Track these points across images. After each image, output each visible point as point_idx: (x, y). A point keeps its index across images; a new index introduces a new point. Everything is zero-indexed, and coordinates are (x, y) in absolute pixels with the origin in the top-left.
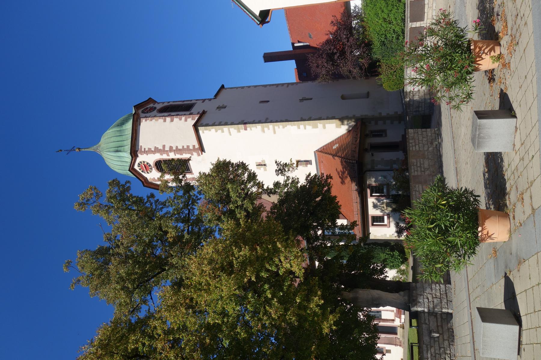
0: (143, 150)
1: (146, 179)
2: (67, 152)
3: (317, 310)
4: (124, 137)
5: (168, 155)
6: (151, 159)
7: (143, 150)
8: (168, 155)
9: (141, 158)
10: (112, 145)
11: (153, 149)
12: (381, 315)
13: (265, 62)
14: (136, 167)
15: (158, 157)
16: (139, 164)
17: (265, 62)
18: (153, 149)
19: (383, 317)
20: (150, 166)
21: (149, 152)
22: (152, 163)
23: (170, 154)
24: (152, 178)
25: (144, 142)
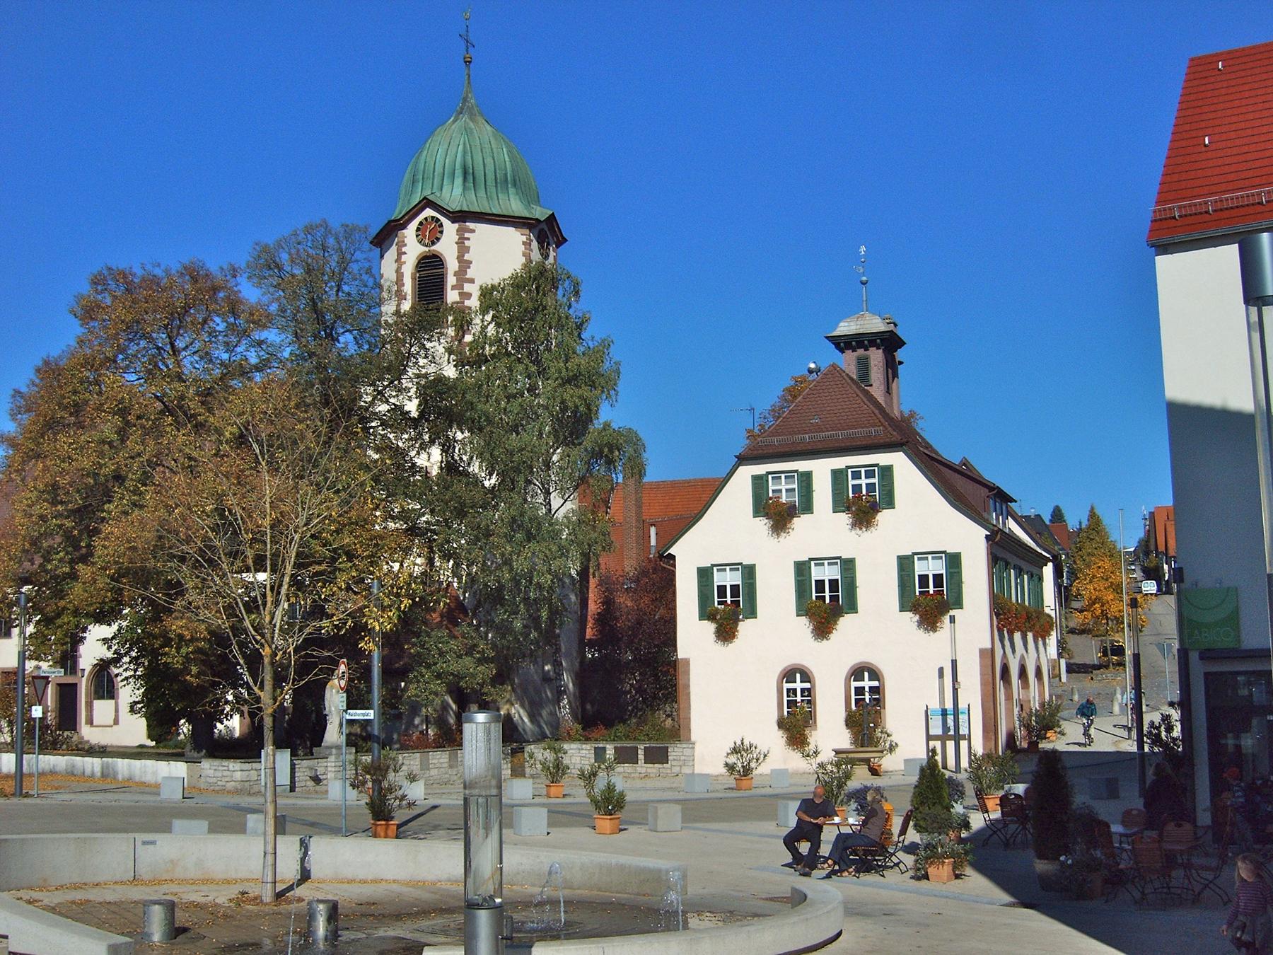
0: (467, 235)
1: (404, 226)
2: (471, 48)
3: (459, 433)
4: (494, 190)
5: (453, 288)
6: (447, 247)
7: (467, 235)
8: (453, 288)
9: (450, 228)
10: (478, 159)
11: (467, 257)
12: (102, 698)
13: (899, 557)
14: (428, 212)
15: (452, 265)
16: (438, 220)
17: (899, 557)
18: (467, 257)
19: (98, 704)
20: (433, 243)
21: (463, 249)
22: (437, 248)
23: (456, 292)
24: (406, 241)
25: (482, 233)
